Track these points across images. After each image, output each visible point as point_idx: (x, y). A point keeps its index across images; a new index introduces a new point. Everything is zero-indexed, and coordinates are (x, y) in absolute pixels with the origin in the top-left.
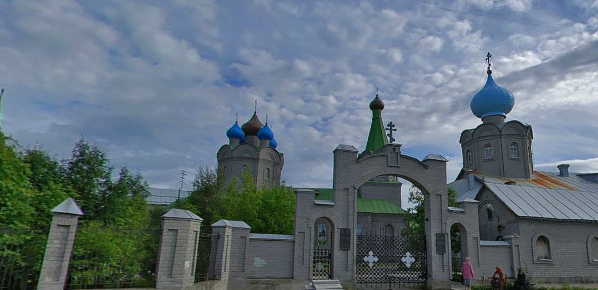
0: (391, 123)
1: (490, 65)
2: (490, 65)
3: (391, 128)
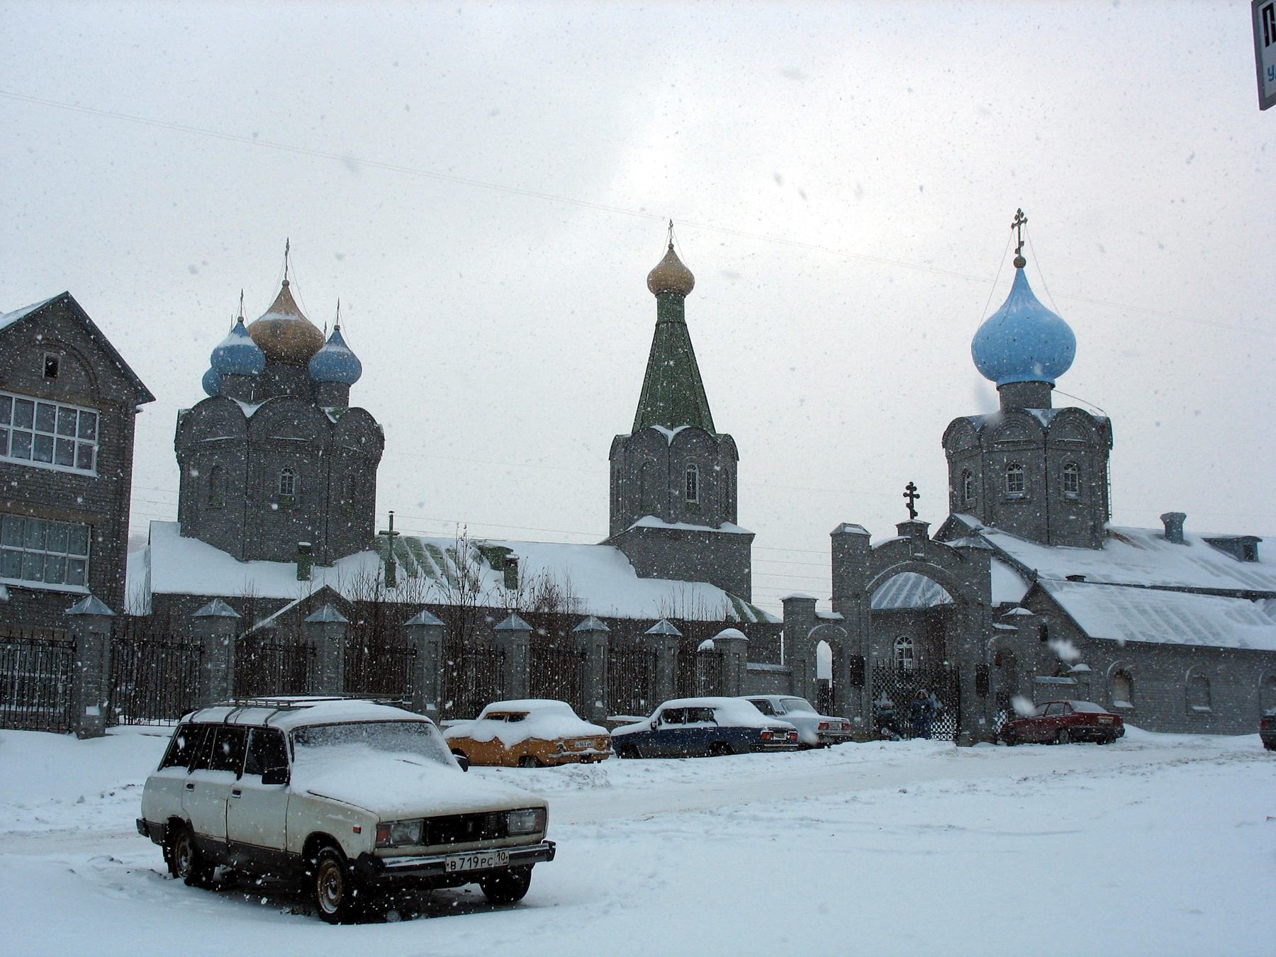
0: (911, 483)
1: (1021, 244)
2: (1021, 244)
3: (911, 492)
